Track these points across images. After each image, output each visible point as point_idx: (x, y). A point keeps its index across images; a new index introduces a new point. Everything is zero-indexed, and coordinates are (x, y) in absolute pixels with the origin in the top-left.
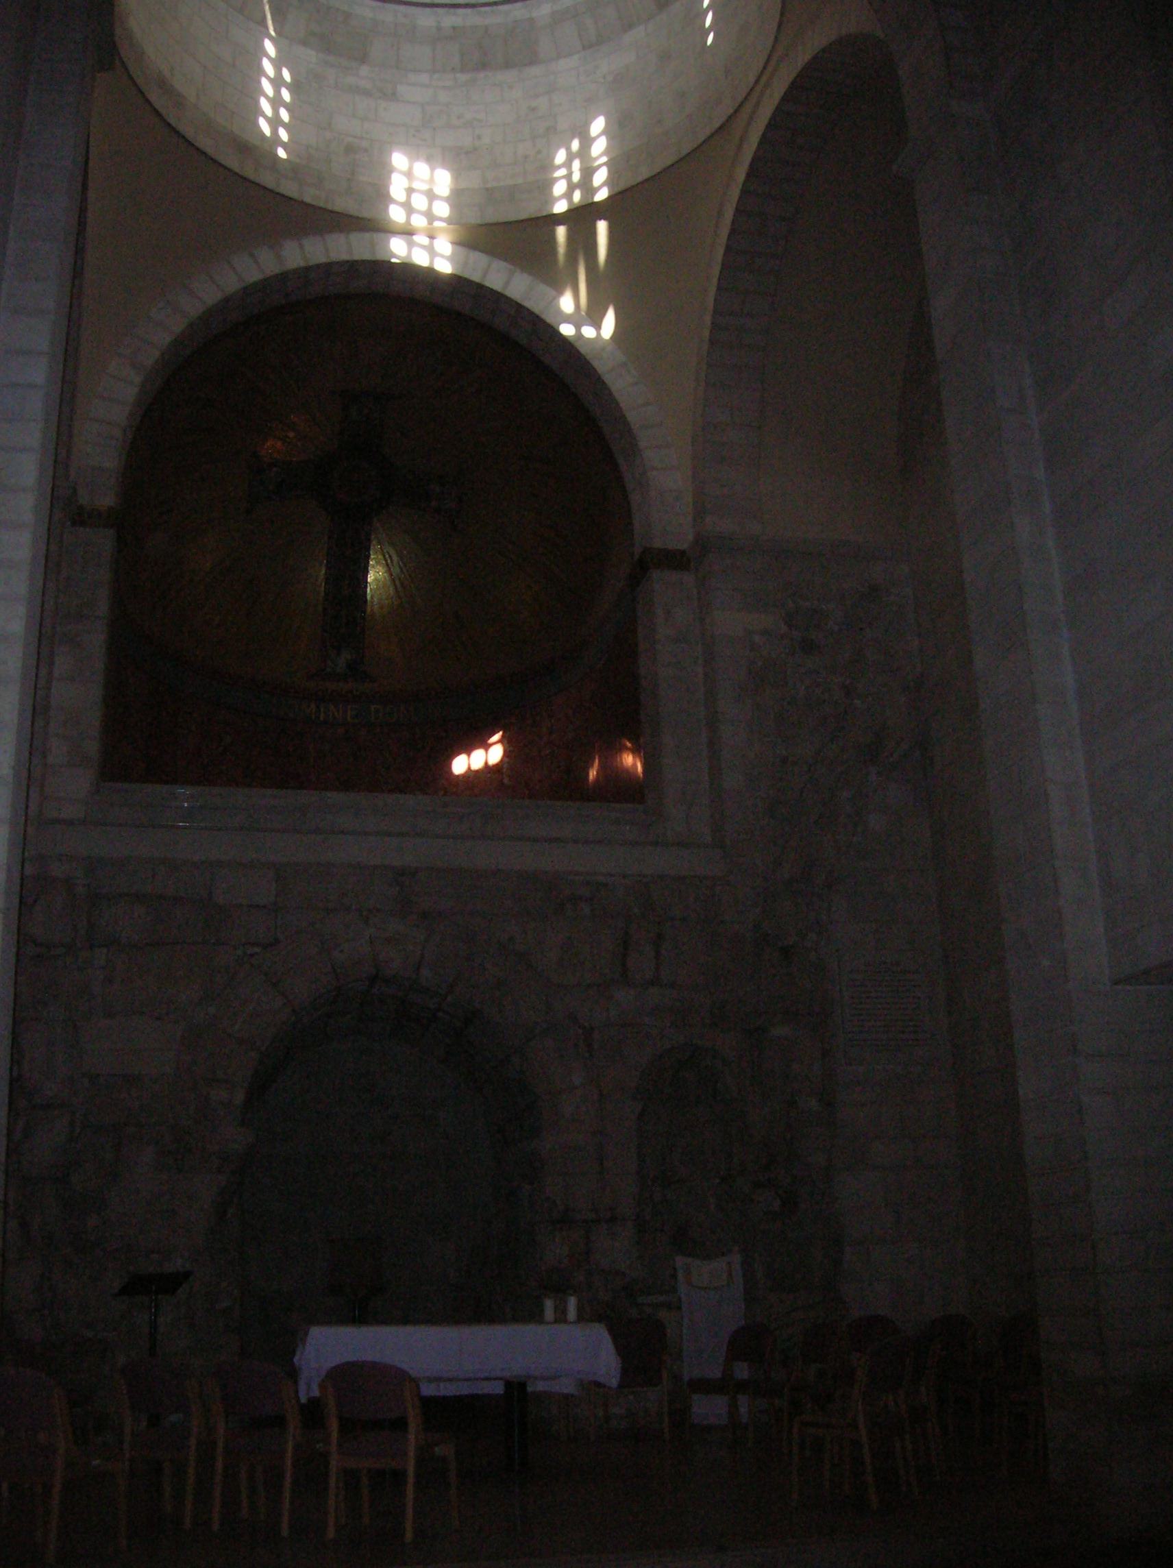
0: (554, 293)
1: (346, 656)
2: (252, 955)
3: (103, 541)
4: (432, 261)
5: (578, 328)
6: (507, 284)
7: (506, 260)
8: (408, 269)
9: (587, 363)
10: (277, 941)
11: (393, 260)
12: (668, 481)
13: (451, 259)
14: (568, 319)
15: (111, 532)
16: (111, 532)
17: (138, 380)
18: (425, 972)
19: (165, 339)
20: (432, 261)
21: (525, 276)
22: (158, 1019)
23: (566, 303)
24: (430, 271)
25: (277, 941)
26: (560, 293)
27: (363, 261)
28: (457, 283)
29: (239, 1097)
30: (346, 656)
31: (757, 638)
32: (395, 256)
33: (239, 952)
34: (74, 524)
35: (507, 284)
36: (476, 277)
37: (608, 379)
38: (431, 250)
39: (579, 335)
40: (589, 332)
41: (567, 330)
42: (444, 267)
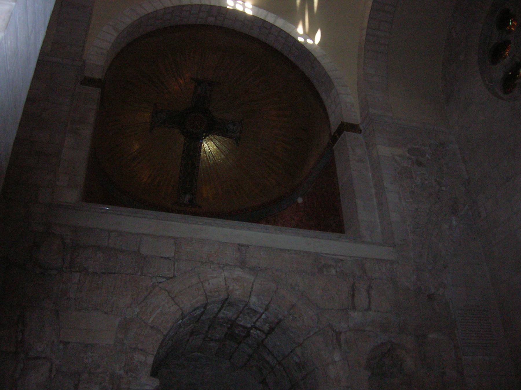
0: (294, 27)
1: (188, 197)
2: (160, 283)
3: (95, 92)
4: (244, 9)
5: (305, 40)
6: (275, 21)
7: (273, 13)
8: (234, 12)
9: (310, 52)
10: (174, 276)
11: (228, 7)
12: (346, 100)
13: (252, 9)
14: (301, 36)
15: (99, 90)
16: (99, 90)
17: (116, 34)
18: (254, 299)
19: (129, 21)
20: (244, 9)
21: (282, 19)
22: (106, 313)
23: (300, 30)
24: (243, 14)
25: (174, 276)
26: (296, 26)
27: (215, 6)
28: (254, 19)
29: (150, 360)
30: (188, 197)
31: (397, 158)
32: (228, 5)
33: (154, 280)
34: (81, 84)
35: (275, 21)
36: (262, 17)
37: (319, 59)
38: (244, 7)
39: (306, 42)
40: (310, 41)
41: (301, 40)
42: (249, 12)
